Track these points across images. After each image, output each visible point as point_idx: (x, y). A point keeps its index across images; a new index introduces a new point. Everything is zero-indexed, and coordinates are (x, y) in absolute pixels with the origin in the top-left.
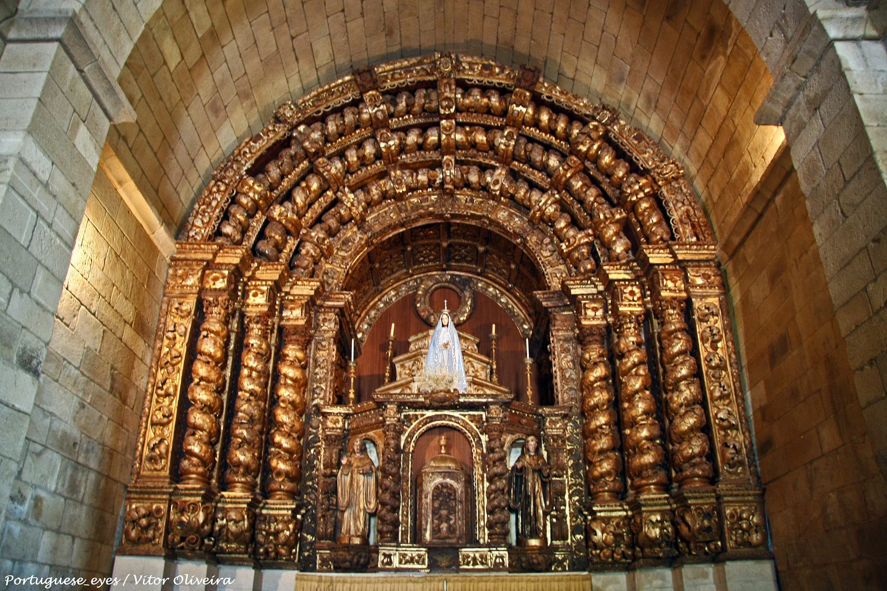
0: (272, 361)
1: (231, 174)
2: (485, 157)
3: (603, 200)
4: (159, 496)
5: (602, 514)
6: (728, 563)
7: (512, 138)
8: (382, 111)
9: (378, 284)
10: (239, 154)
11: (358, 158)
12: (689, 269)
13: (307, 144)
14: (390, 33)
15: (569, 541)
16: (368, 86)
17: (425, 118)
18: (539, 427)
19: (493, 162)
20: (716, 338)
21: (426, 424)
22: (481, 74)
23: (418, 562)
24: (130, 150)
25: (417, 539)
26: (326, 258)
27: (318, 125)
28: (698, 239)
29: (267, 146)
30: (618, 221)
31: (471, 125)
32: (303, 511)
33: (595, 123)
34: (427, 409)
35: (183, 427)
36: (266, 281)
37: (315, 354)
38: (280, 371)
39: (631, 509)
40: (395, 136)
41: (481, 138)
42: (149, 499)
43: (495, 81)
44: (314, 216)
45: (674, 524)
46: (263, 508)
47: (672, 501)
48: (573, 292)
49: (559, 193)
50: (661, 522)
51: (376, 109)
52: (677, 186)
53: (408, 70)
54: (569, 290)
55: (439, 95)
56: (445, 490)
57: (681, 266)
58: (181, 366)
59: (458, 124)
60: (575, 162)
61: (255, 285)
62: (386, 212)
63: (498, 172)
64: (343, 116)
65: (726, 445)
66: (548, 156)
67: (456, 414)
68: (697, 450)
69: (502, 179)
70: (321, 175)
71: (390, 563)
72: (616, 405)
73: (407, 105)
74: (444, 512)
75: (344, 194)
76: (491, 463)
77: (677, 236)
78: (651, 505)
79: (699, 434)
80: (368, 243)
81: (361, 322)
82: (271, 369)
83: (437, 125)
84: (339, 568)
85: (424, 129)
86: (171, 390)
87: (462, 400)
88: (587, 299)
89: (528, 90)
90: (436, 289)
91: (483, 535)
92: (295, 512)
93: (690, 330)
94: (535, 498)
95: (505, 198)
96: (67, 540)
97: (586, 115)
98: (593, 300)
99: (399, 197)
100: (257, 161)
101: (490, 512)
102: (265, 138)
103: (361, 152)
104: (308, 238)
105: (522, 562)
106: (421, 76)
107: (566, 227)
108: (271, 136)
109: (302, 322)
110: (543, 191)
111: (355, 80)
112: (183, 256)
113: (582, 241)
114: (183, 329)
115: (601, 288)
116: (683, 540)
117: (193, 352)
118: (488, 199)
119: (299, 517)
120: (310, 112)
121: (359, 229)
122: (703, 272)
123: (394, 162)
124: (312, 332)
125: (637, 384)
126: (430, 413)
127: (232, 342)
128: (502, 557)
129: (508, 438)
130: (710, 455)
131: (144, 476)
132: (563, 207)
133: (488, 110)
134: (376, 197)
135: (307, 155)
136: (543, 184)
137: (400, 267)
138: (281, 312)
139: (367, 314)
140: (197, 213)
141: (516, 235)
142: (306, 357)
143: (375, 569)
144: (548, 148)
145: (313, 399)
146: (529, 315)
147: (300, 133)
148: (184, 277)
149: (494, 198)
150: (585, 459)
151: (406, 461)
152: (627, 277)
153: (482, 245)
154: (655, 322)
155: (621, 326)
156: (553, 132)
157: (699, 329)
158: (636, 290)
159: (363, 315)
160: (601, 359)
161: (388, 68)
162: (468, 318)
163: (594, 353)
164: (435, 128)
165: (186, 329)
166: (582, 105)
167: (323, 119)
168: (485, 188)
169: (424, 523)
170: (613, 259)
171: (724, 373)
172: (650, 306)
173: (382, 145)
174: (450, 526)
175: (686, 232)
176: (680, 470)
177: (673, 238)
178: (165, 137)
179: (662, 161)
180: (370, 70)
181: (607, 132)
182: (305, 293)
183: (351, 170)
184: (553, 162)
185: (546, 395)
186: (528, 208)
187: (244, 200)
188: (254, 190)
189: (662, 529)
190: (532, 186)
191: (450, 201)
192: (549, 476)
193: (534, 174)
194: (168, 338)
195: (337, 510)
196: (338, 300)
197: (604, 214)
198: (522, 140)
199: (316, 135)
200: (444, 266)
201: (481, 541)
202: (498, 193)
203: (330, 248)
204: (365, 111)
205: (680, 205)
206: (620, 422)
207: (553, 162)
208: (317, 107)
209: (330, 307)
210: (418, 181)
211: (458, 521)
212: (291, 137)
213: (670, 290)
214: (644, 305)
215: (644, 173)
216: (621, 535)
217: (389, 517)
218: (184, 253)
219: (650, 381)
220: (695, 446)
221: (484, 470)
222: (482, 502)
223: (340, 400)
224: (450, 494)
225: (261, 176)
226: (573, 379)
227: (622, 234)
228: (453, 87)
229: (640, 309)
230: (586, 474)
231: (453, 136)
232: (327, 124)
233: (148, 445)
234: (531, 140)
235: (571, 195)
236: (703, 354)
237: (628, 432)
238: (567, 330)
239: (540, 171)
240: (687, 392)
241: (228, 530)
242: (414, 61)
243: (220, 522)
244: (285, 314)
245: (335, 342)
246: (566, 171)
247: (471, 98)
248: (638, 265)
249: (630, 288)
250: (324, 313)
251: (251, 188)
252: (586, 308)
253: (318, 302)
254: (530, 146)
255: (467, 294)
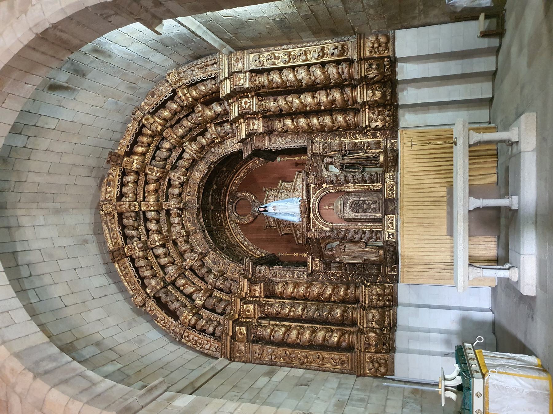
0: (284, 301)
1: (178, 330)
2: (163, 184)
3: (190, 117)
4: (362, 358)
5: (367, 122)
6: (396, 56)
7: (153, 169)
8: (137, 245)
9: (234, 245)
10: (165, 326)
11: (165, 257)
12: (233, 70)
13: (158, 287)
14: (86, 241)
15: (381, 139)
16: (122, 253)
17: (140, 219)
18: (318, 156)
19: (167, 180)
20: (273, 57)
21: (317, 217)
22: (114, 187)
23: (393, 220)
24: (172, 385)
25: (379, 221)
26: (224, 273)
27: (146, 281)
28: (215, 63)
29: (160, 310)
30: (203, 109)
31: (144, 193)
32: (365, 282)
33: (144, 119)
34: (309, 216)
35: (324, 346)
36: (240, 305)
37: (279, 278)
38: (290, 296)
39: (365, 106)
40: (152, 237)
41: (152, 187)
42: (364, 364)
43: (118, 178)
44: (200, 281)
45: (374, 83)
46: (365, 303)
47: (362, 84)
48: (244, 137)
49: (185, 142)
50: (372, 90)
51: (136, 248)
52: (183, 74)
53: (111, 230)
54: (243, 139)
55: (127, 212)
56: (353, 206)
57: (232, 74)
58: (291, 350)
59: (144, 200)
60: (167, 132)
61: (243, 312)
62: (196, 241)
63: (172, 177)
64: (140, 267)
65: (333, 54)
66: (163, 148)
67: (312, 201)
68: (335, 70)
69: (177, 175)
70: (176, 278)
71: (393, 234)
72: (307, 114)
73: (134, 230)
74: (365, 206)
75: (187, 265)
76: (338, 182)
77: (213, 76)
78: (363, 96)
79: (326, 69)
80: (214, 250)
81: (255, 254)
82: (289, 301)
83: (144, 212)
84: (397, 262)
85: (146, 220)
86: (304, 354)
87: (305, 198)
88: (248, 129)
89: (123, 160)
90: (236, 213)
91: (378, 186)
92: (366, 286)
93: (268, 71)
94: (358, 158)
95: (187, 173)
96: (389, 402)
97: (139, 125)
98: (249, 125)
99: (188, 234)
100: (169, 316)
101: (365, 182)
102: (155, 312)
103: (162, 256)
104: (213, 284)
105: (392, 165)
106: (115, 222)
107: (205, 139)
108: (154, 308)
109: (262, 285)
110: (184, 151)
111: (118, 261)
112: (228, 354)
113: (214, 130)
114: (270, 350)
115: (242, 121)
116: (383, 79)
117: (282, 343)
118: (188, 183)
119: (368, 284)
120: (138, 286)
121: (206, 256)
122: (235, 62)
123: (167, 237)
124: (266, 279)
125: (296, 102)
126: (312, 215)
127: (275, 323)
128: (390, 176)
129: (325, 173)
130: (338, 63)
131: (352, 367)
132: (194, 139)
133: (136, 182)
134: (188, 247)
135: (165, 287)
136: (180, 151)
137: (224, 233)
138: (257, 297)
139: (251, 251)
140: (202, 348)
141: (209, 167)
142: (281, 282)
143: (396, 243)
144: (158, 148)
145: (304, 278)
146: (251, 160)
147: (151, 292)
148: (240, 351)
149: (188, 180)
150: (335, 131)
151: (337, 227)
152: (236, 106)
153: (212, 186)
154: (262, 91)
155: (264, 110)
156: (149, 145)
157: (267, 66)
158: (244, 100)
159: (251, 253)
160: (282, 121)
161: (110, 242)
162: (253, 195)
163: (278, 125)
164: (147, 214)
165: (270, 348)
166: (133, 127)
167: (142, 279)
168: (182, 184)
169: (371, 217)
170: (226, 113)
171: (292, 53)
172: (253, 94)
173: (157, 244)
174: (372, 203)
175: (210, 71)
176: (345, 80)
177: (214, 78)
178: (162, 368)
179: (168, 81)
180: (112, 252)
181: (149, 113)
182: (246, 284)
183: (173, 261)
184: (167, 145)
185: (303, 151)
186: (194, 160)
187: (193, 321)
188: (187, 316)
189: (376, 90)
190: (180, 157)
191: (189, 205)
192: (346, 151)
193: (174, 157)
194: (275, 359)
195: (364, 264)
196: (249, 266)
197: (199, 117)
198: (154, 162)
199: (153, 282)
200: (223, 208)
201: (380, 187)
202: (185, 178)
203: (219, 272)
204: (137, 254)
205: (194, 73)
206: (317, 112)
207: (167, 145)
208: (135, 283)
209: (253, 270)
210: (179, 223)
211: (370, 199)
212: (154, 297)
213: (245, 82)
214: (252, 97)
215: (174, 92)
216: (379, 112)
217: (368, 235)
218: (227, 353)
219: (296, 95)
220: (332, 70)
221: (343, 186)
222: (360, 187)
223: (305, 264)
224: (356, 203)
225: (178, 313)
226: (292, 137)
227: (210, 107)
228: (122, 203)
229: (254, 99)
230: (344, 130)
231: (152, 203)
232: (146, 276)
233: (334, 366)
234: (153, 158)
235: (186, 135)
236: (281, 65)
237: (323, 108)
238: (264, 140)
239: (172, 153)
240: (302, 74)
241: (378, 321)
242: (105, 227)
243: (374, 325)
244: (257, 294)
245: (272, 267)
246: (173, 137)
247: (128, 192)
248: (230, 99)
249: (243, 104)
250: (255, 273)
251: (186, 318)
252: (253, 130)
253: (250, 277)
254: (157, 158)
255: (239, 195)
